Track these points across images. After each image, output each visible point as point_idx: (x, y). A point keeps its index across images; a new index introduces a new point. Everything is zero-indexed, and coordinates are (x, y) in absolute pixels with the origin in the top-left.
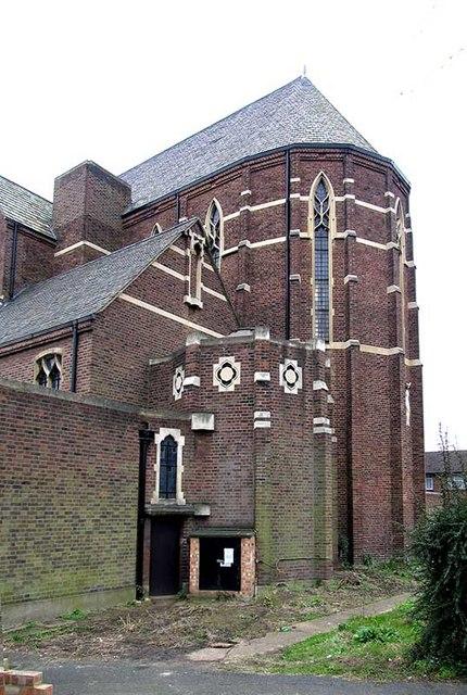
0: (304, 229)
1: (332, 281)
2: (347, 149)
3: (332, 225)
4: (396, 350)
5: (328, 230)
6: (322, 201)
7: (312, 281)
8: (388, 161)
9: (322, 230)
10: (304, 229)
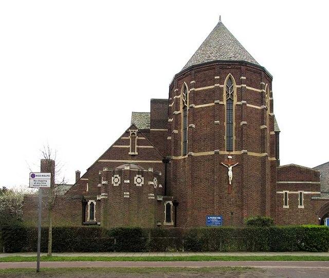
0: (222, 100)
1: (234, 124)
2: (242, 63)
3: (235, 99)
4: (265, 154)
5: (233, 101)
6: (230, 87)
7: (225, 123)
8: (263, 68)
9: (230, 101)
10: (222, 100)
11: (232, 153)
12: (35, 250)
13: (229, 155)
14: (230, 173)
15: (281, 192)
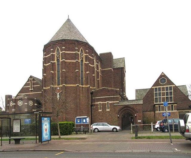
2: (78, 41)
4: (88, 86)
5: (83, 61)
11: (59, 86)
12: (58, 135)
13: (58, 87)
14: (58, 96)
15: (97, 103)
